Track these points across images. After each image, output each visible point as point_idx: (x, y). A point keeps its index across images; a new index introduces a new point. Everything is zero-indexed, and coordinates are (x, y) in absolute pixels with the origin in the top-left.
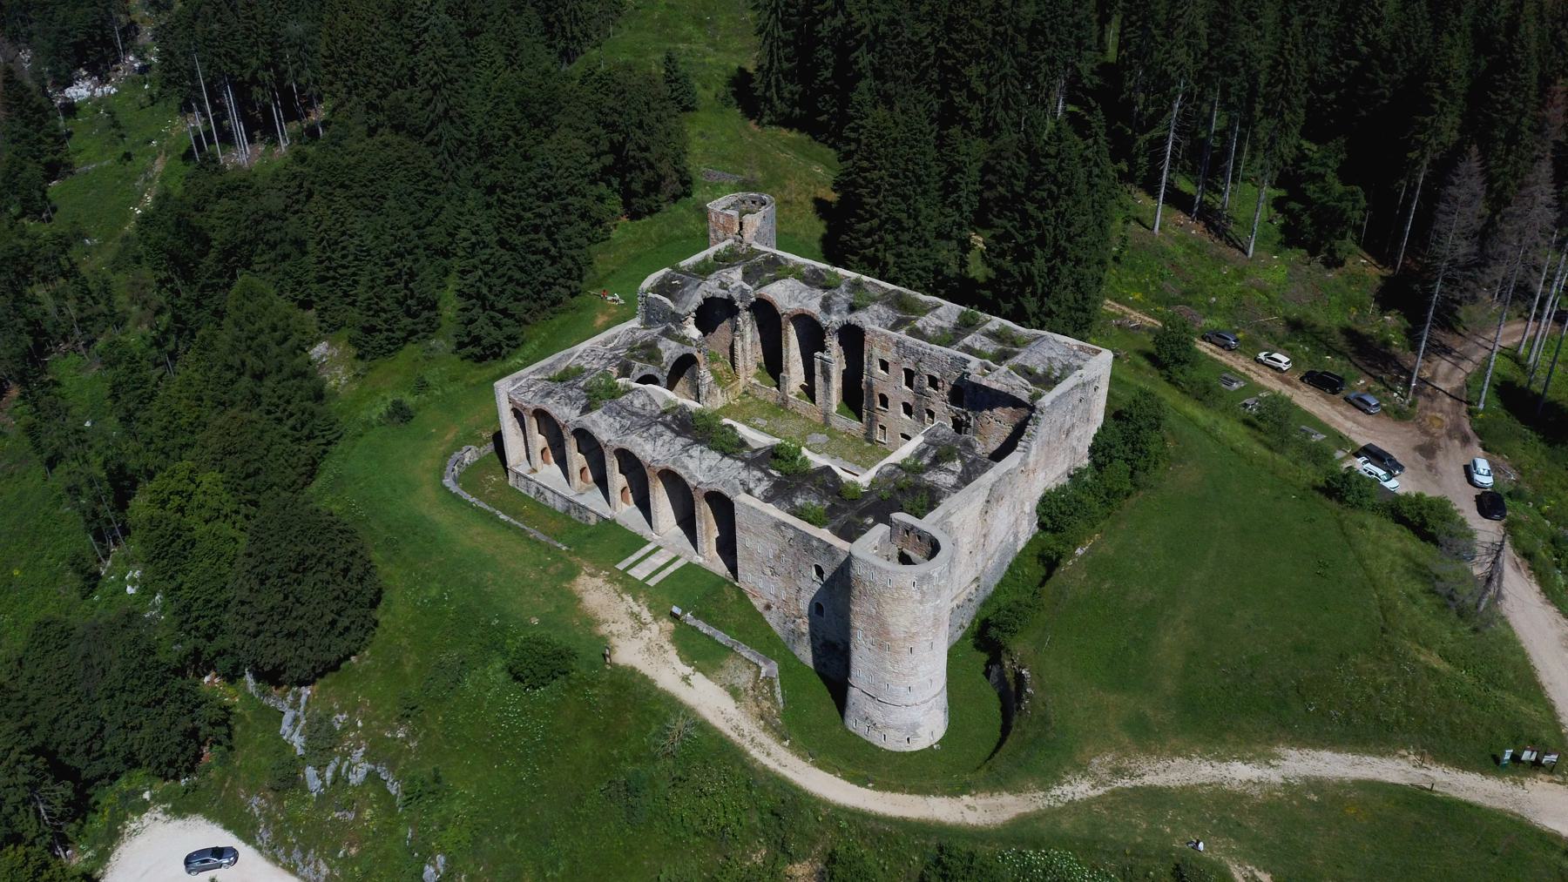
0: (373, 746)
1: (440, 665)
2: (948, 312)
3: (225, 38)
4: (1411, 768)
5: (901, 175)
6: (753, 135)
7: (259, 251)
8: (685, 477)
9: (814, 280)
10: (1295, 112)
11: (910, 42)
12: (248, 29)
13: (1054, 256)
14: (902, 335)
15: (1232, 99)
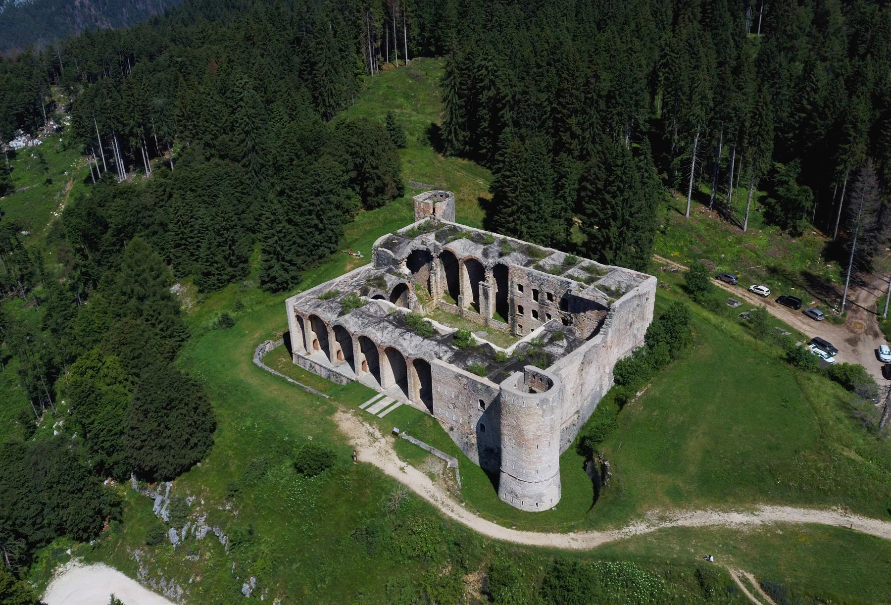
0: (211, 515)
1: (253, 464)
2: (559, 257)
3: (114, 108)
4: (839, 517)
5: (530, 180)
6: (440, 162)
7: (138, 230)
8: (401, 351)
9: (477, 239)
10: (767, 143)
11: (535, 104)
12: (128, 102)
13: (622, 225)
14: (531, 269)
15: (730, 136)
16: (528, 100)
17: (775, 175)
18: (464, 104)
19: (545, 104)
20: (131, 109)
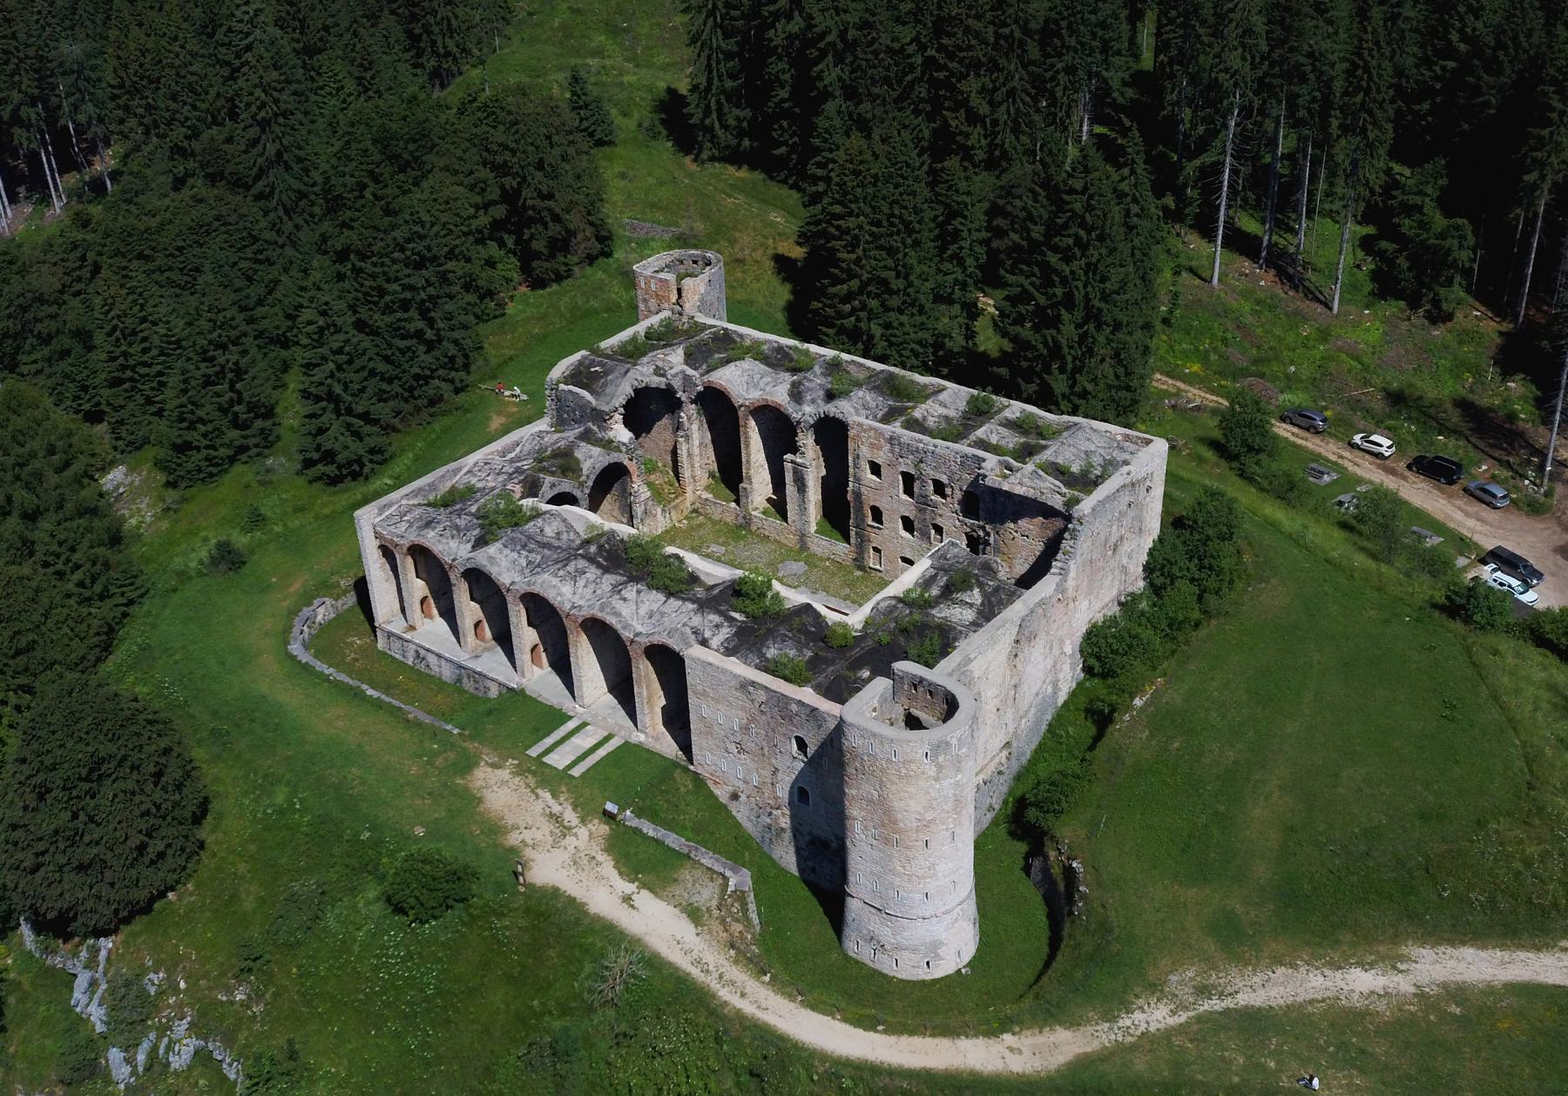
0: (202, 1014)
1: (293, 898)
2: (954, 397)
5: (885, 223)
6: (690, 175)
7: (27, 348)
8: (618, 627)
9: (778, 360)
10: (1380, 128)
11: (889, 50)
13: (1086, 320)
14: (896, 428)
15: (1302, 113)
16: (874, 40)
17: (1395, 193)
18: (735, 49)
19: (911, 49)
20: (12, 66)
